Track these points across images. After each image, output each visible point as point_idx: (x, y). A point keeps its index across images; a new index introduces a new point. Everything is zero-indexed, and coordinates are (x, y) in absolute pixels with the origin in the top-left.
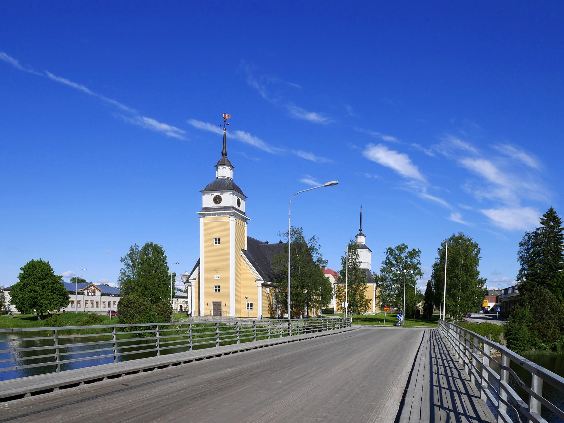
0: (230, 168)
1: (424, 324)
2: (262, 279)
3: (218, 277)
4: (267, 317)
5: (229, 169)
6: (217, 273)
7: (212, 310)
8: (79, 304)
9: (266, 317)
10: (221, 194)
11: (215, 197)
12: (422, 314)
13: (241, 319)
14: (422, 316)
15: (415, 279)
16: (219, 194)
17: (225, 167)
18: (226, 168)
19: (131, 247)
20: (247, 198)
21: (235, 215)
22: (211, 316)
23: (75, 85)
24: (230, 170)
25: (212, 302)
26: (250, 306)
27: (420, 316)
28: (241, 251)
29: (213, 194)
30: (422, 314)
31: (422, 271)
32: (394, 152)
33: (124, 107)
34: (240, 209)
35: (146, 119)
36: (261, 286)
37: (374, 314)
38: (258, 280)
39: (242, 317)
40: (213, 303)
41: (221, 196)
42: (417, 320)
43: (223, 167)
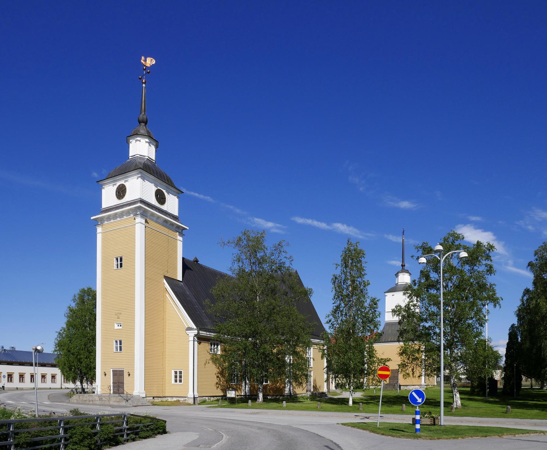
0: (147, 140)
1: (506, 412)
2: (195, 327)
3: (121, 326)
4: (213, 397)
5: (146, 142)
6: (118, 318)
7: (112, 385)
8: (45, 378)
9: (210, 397)
10: (125, 181)
11: (118, 188)
12: (502, 387)
13: (164, 399)
14: (501, 391)
15: (484, 311)
16: (122, 182)
17: (138, 139)
18: (140, 141)
19: (75, 294)
20: (183, 193)
21: (144, 214)
22: (110, 394)
23: (202, 196)
24: (147, 144)
25: (112, 370)
26: (179, 377)
27: (498, 391)
28: (165, 281)
29: (115, 184)
30: (502, 387)
31: (498, 295)
32: (479, 231)
33: (238, 211)
34: (164, 207)
35: (256, 219)
36: (194, 341)
37: (423, 388)
38: (189, 329)
39: (166, 395)
40: (113, 371)
41: (125, 184)
42: (492, 399)
43: (136, 139)
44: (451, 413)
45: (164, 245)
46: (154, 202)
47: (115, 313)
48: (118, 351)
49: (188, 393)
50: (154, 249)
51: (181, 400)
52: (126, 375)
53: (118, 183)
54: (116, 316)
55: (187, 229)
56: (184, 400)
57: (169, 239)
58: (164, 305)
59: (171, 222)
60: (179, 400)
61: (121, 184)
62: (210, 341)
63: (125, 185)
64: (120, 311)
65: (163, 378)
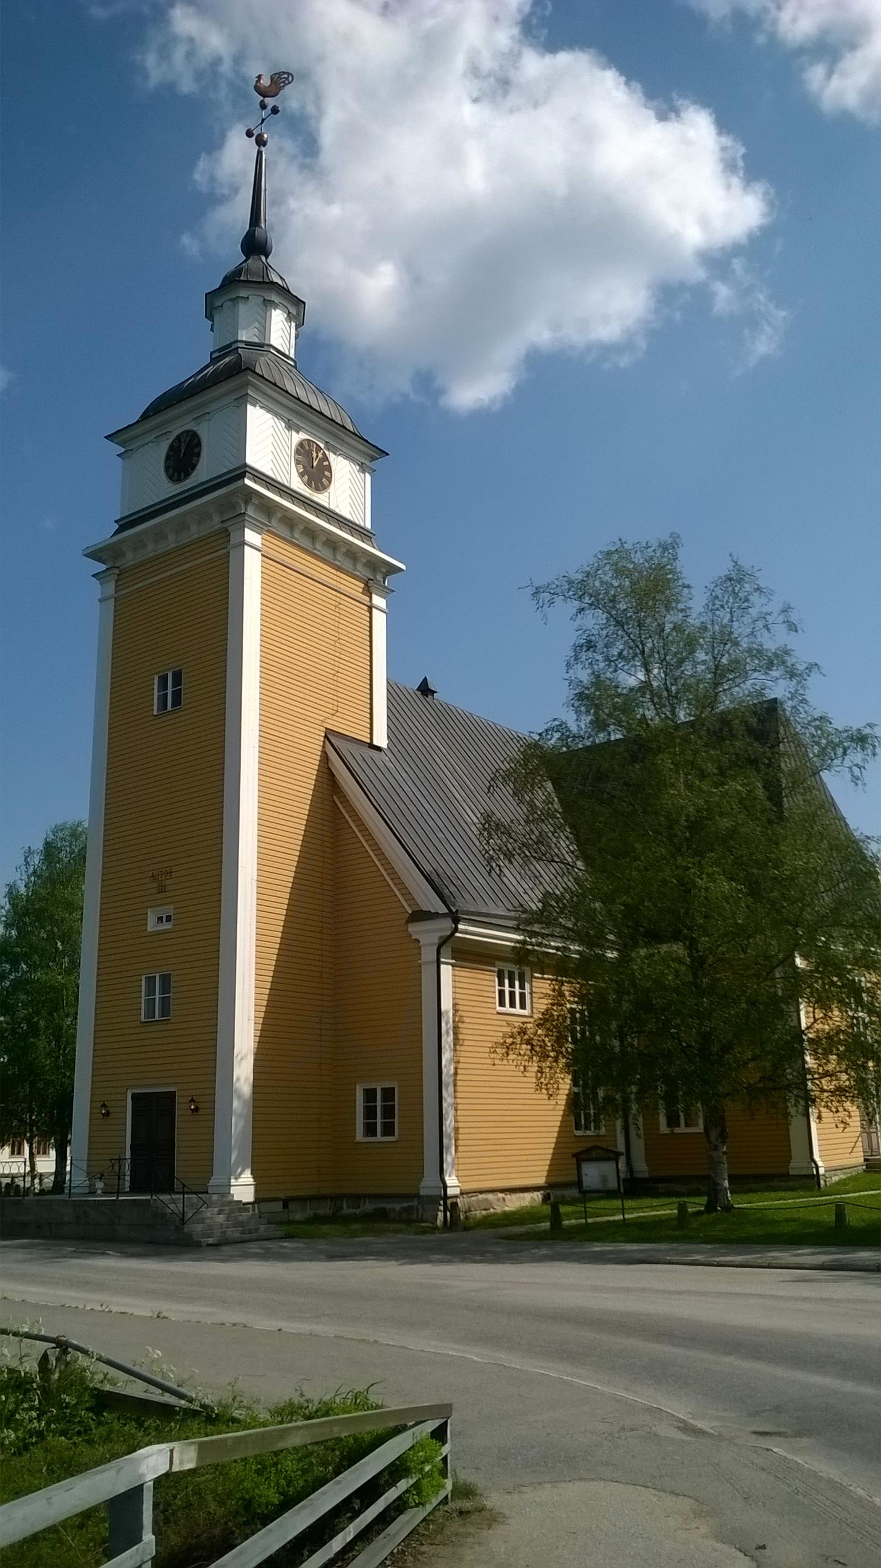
3: (169, 918)
34: (320, 498)
44: (369, 558)
45: (324, 624)
46: (297, 484)
47: (150, 874)
48: (157, 1018)
49: (420, 1180)
50: (306, 615)
51: (394, 1210)
52: (181, 1109)
53: (177, 429)
54: (155, 885)
55: (401, 570)
56: (405, 1209)
57: (342, 602)
58: (320, 952)
59: (287, 509)
60: (384, 1209)
61: (183, 432)
62: (497, 963)
63: (199, 432)
64: (166, 864)
65: (337, 711)
